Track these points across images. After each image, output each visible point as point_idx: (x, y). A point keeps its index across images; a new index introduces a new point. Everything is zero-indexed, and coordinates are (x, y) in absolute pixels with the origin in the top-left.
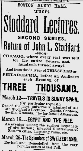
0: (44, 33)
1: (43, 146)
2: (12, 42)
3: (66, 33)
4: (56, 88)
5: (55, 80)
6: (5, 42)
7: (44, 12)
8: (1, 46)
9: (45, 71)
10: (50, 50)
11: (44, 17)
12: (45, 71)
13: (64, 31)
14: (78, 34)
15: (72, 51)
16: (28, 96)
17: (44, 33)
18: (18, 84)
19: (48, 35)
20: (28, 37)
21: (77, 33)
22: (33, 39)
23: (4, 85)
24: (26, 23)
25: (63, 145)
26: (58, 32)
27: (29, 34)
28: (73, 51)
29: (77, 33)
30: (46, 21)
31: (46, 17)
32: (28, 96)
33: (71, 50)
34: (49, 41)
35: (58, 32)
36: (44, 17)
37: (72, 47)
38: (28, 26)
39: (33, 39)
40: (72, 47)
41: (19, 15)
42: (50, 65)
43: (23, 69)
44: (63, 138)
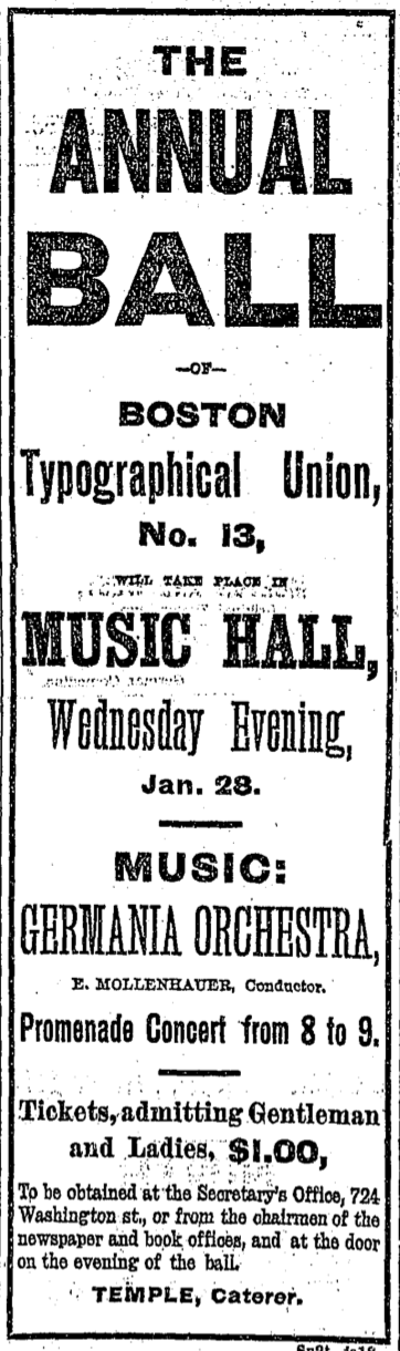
0: (232, 750)
2: (66, 1208)
3: (228, 953)
4: (106, 642)
6: (24, 1015)
8: (78, 11)
11: (113, 1156)
13: (292, 744)
16: (94, 1289)
17: (232, 750)
20: (224, 1292)
21: (372, 1042)
22: (263, 424)
23: (96, 1292)
24: (176, 722)
26: (173, 1039)
27: (218, 893)
29: (372, 1042)
32: (94, 1289)
33: (132, 486)
35: (173, 1039)
36: (113, 1156)
37: (103, 1026)
38: (180, 731)
39: (263, 424)
40: (103, 1026)
41: (167, 698)
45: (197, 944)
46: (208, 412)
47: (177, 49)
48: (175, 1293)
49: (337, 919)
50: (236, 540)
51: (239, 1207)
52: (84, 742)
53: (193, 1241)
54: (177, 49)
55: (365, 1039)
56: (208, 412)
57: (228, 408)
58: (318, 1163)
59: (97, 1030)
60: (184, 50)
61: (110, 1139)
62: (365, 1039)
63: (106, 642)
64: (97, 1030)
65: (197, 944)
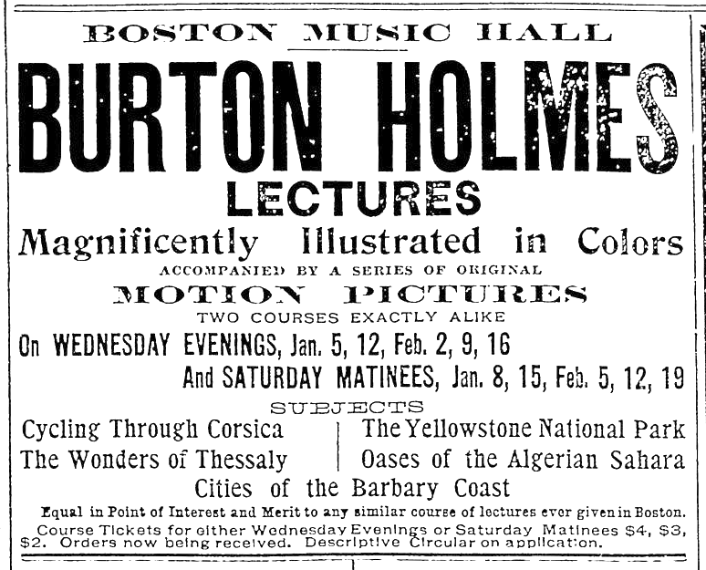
1: (439, 445)
4: (132, 343)
5: (458, 270)
7: (528, 294)
9: (472, 516)
10: (509, 164)
12: (472, 516)
14: (425, 353)
15: (463, 386)
18: (122, 66)
19: (390, 190)
21: (422, 352)
25: (542, 237)
28: (466, 385)
29: (422, 352)
30: (394, 245)
31: (396, 252)
34: (105, 538)
42: (336, 271)
43: (571, 528)
44: (77, 339)
45: (21, 348)
46: (181, 81)
47: (349, 185)
48: (477, 431)
49: (511, 429)
50: (458, 241)
51: (487, 445)
52: (312, 344)
53: (465, 513)
54: (349, 185)
55: (467, 350)
56: (181, 81)
57: (221, 70)
58: (434, 387)
59: (413, 348)
60: (355, 186)
61: (476, 230)
62: (467, 350)
63: (132, 343)
64: (413, 348)
65: (21, 348)
